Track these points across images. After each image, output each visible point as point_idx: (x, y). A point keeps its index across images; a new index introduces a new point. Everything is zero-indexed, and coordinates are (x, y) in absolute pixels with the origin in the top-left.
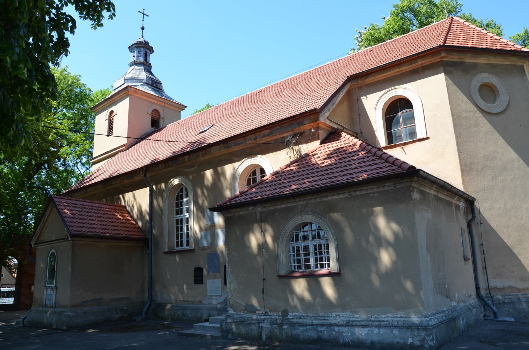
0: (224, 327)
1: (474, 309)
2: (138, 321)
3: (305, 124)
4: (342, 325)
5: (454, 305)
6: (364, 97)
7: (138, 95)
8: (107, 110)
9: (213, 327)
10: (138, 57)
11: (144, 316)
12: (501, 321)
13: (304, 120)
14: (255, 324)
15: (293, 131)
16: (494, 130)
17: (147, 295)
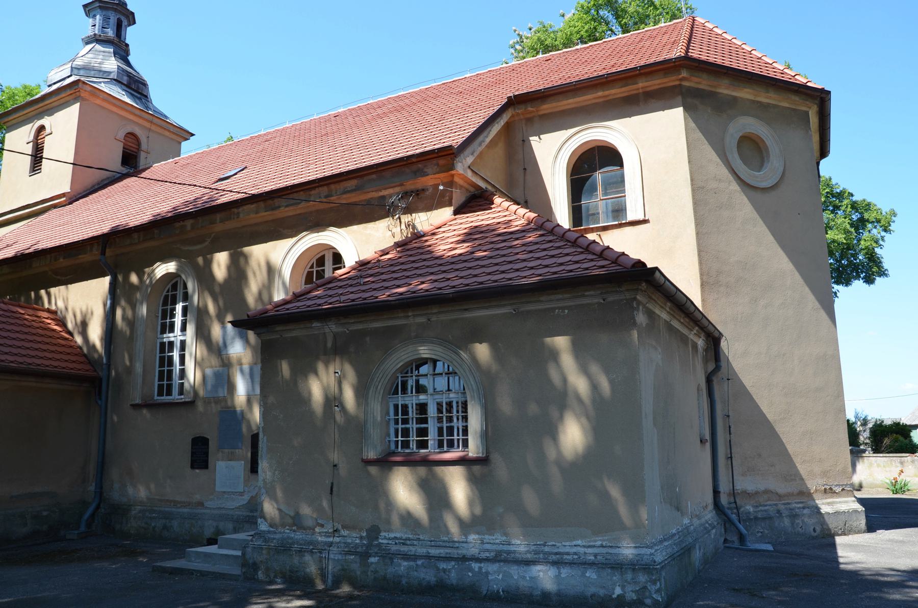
0: (247, 557)
1: (712, 529)
2: (69, 540)
3: (428, 175)
4: (487, 560)
5: (686, 524)
6: (536, 138)
7: (98, 102)
8: (32, 124)
9: (226, 555)
10: (103, 27)
11: (83, 528)
12: (751, 550)
13: (426, 166)
14: (313, 552)
15: (403, 187)
16: (758, 216)
17: (92, 488)
